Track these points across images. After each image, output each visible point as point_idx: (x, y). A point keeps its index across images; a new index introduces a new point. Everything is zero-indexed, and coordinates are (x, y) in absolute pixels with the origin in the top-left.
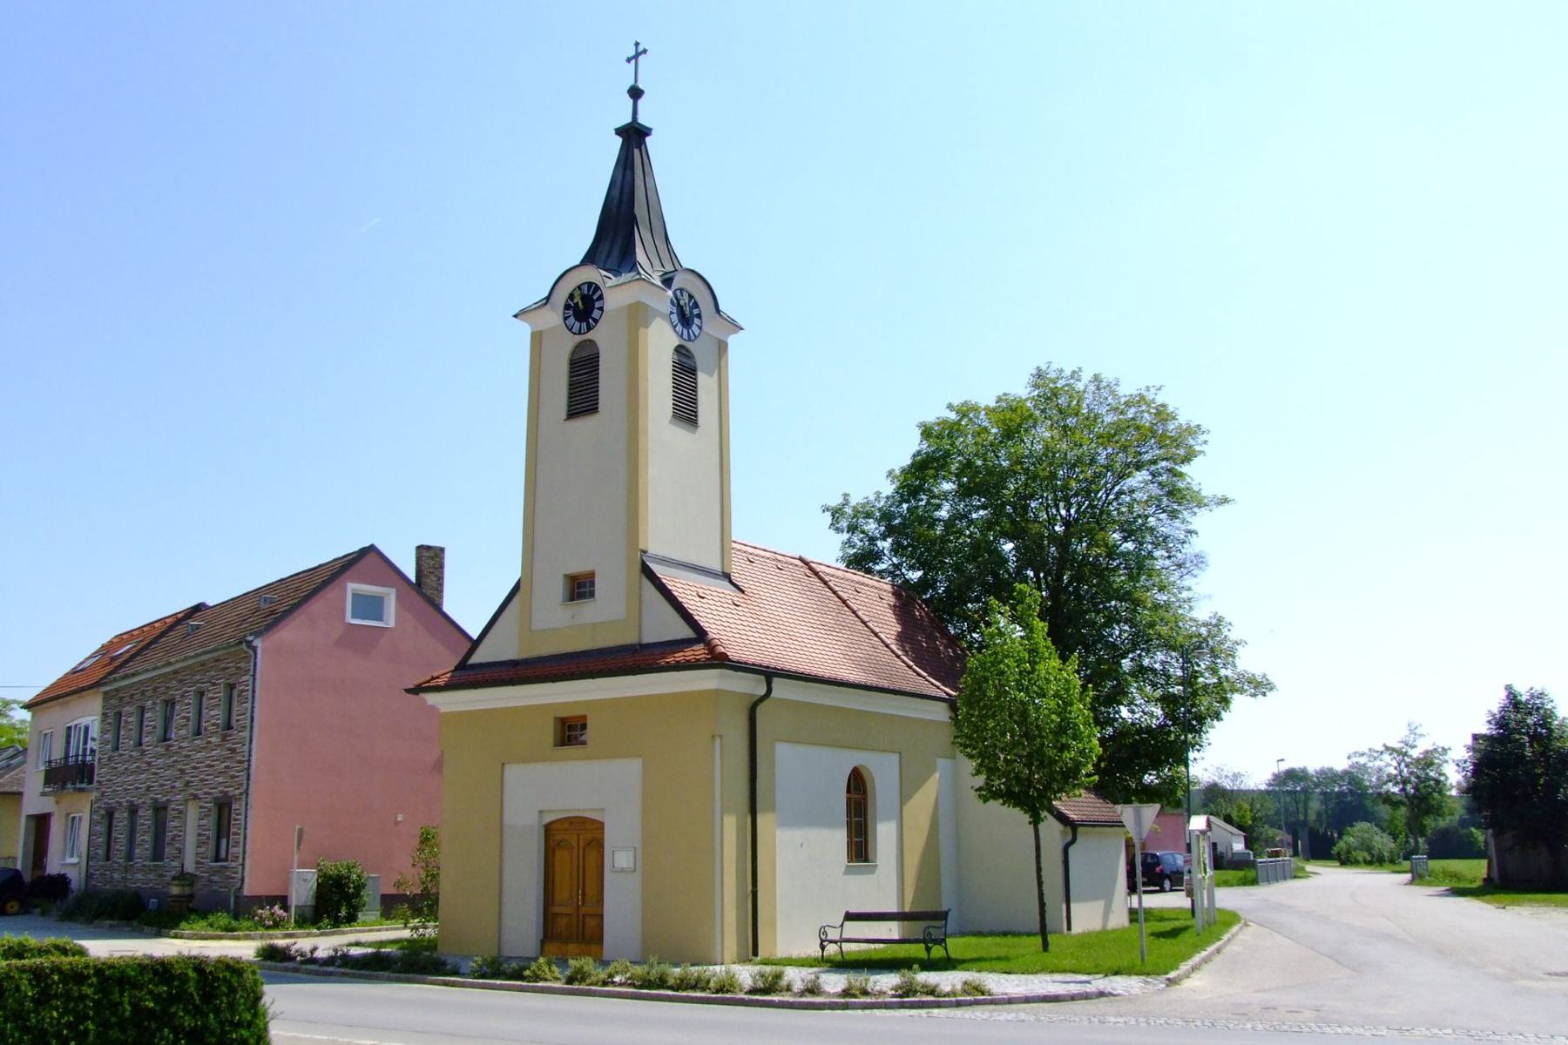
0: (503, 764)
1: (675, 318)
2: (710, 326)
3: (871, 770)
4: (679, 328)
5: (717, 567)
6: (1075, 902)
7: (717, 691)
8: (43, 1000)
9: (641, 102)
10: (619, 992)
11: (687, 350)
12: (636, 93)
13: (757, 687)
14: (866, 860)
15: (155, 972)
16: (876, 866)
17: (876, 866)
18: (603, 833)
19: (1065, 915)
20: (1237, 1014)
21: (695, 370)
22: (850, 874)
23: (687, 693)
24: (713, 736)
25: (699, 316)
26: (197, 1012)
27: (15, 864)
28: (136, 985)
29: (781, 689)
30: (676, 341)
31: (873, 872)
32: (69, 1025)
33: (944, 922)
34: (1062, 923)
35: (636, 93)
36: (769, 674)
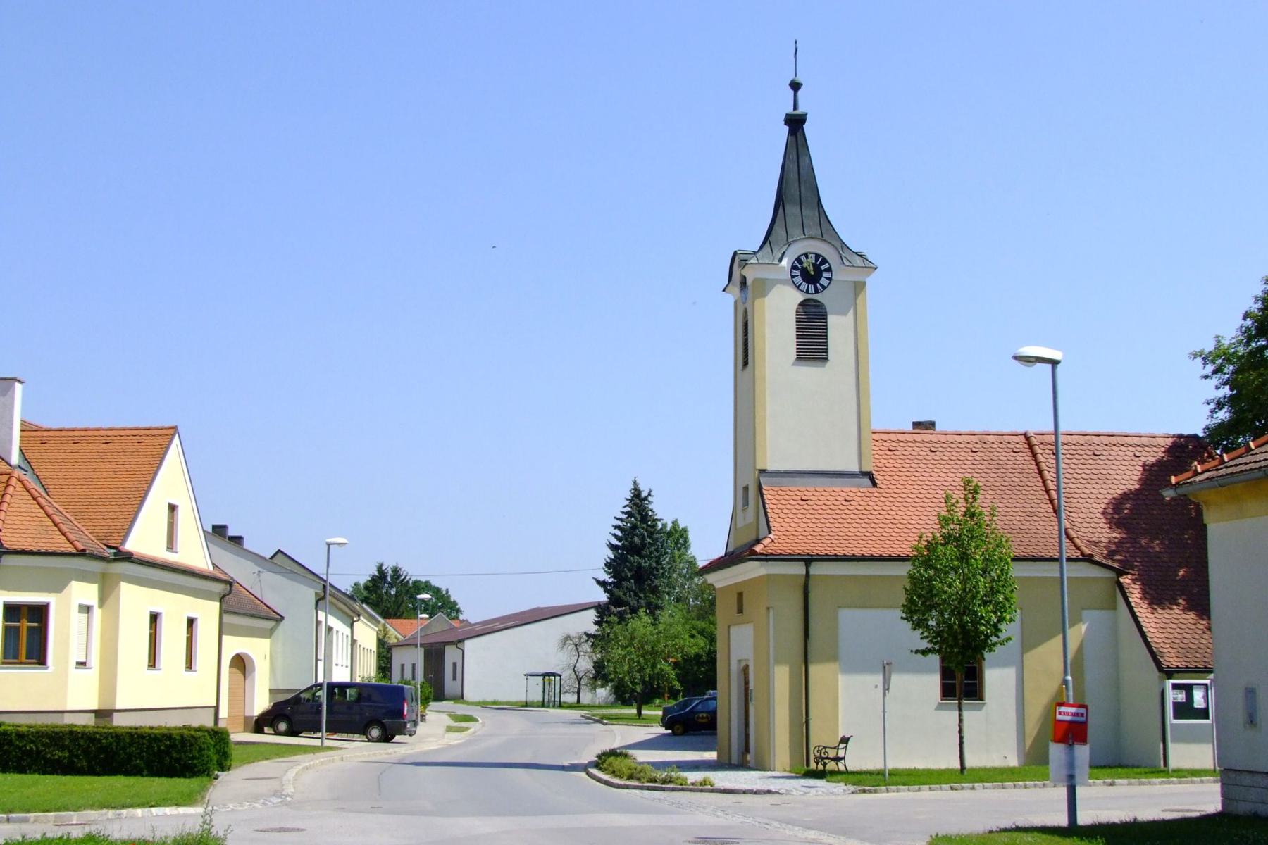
0: (729, 627)
1: (799, 280)
2: (841, 275)
3: (256, 664)
4: (804, 286)
5: (854, 468)
6: (114, 703)
7: (768, 576)
8: (131, 744)
9: (800, 92)
10: (655, 787)
11: (819, 302)
12: (795, 86)
13: (798, 569)
14: (982, 700)
15: (167, 737)
16: (985, 703)
17: (985, 703)
18: (229, 685)
19: (1162, 752)
20: (769, 792)
21: (826, 315)
22: (942, 709)
23: (751, 579)
24: (768, 608)
25: (829, 269)
26: (179, 752)
27: (1063, 699)
28: (161, 741)
29: (817, 569)
30: (800, 297)
31: (980, 709)
32: (138, 753)
33: (845, 745)
34: (1160, 760)
35: (795, 86)
36: (808, 560)
